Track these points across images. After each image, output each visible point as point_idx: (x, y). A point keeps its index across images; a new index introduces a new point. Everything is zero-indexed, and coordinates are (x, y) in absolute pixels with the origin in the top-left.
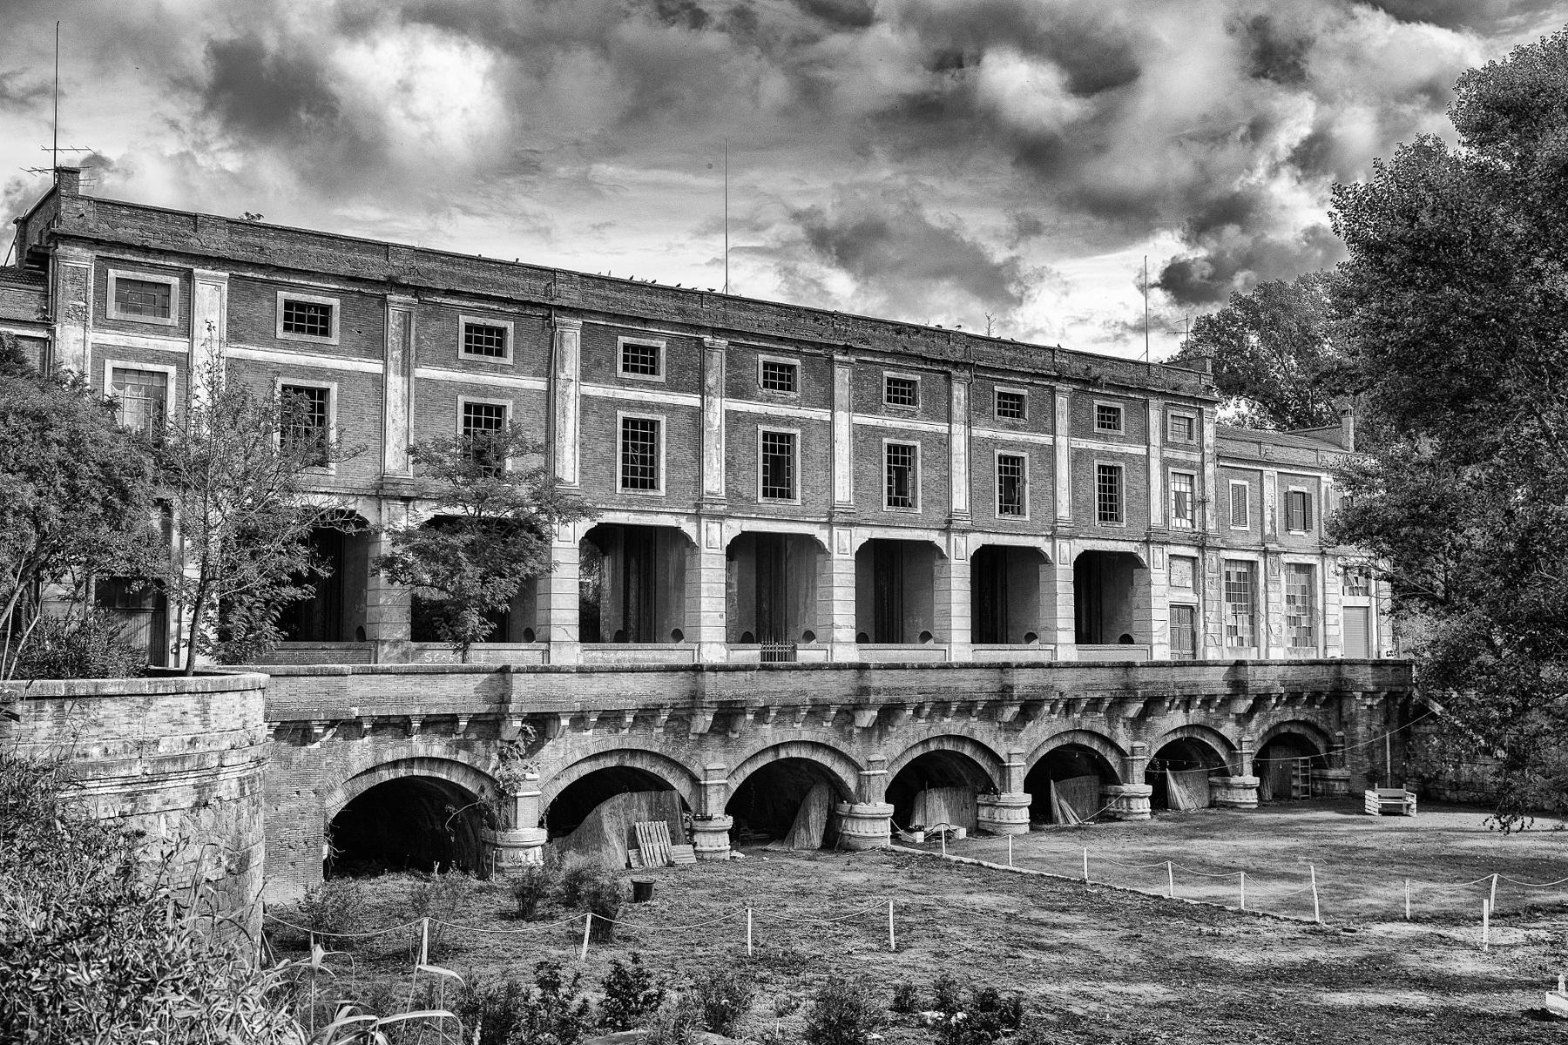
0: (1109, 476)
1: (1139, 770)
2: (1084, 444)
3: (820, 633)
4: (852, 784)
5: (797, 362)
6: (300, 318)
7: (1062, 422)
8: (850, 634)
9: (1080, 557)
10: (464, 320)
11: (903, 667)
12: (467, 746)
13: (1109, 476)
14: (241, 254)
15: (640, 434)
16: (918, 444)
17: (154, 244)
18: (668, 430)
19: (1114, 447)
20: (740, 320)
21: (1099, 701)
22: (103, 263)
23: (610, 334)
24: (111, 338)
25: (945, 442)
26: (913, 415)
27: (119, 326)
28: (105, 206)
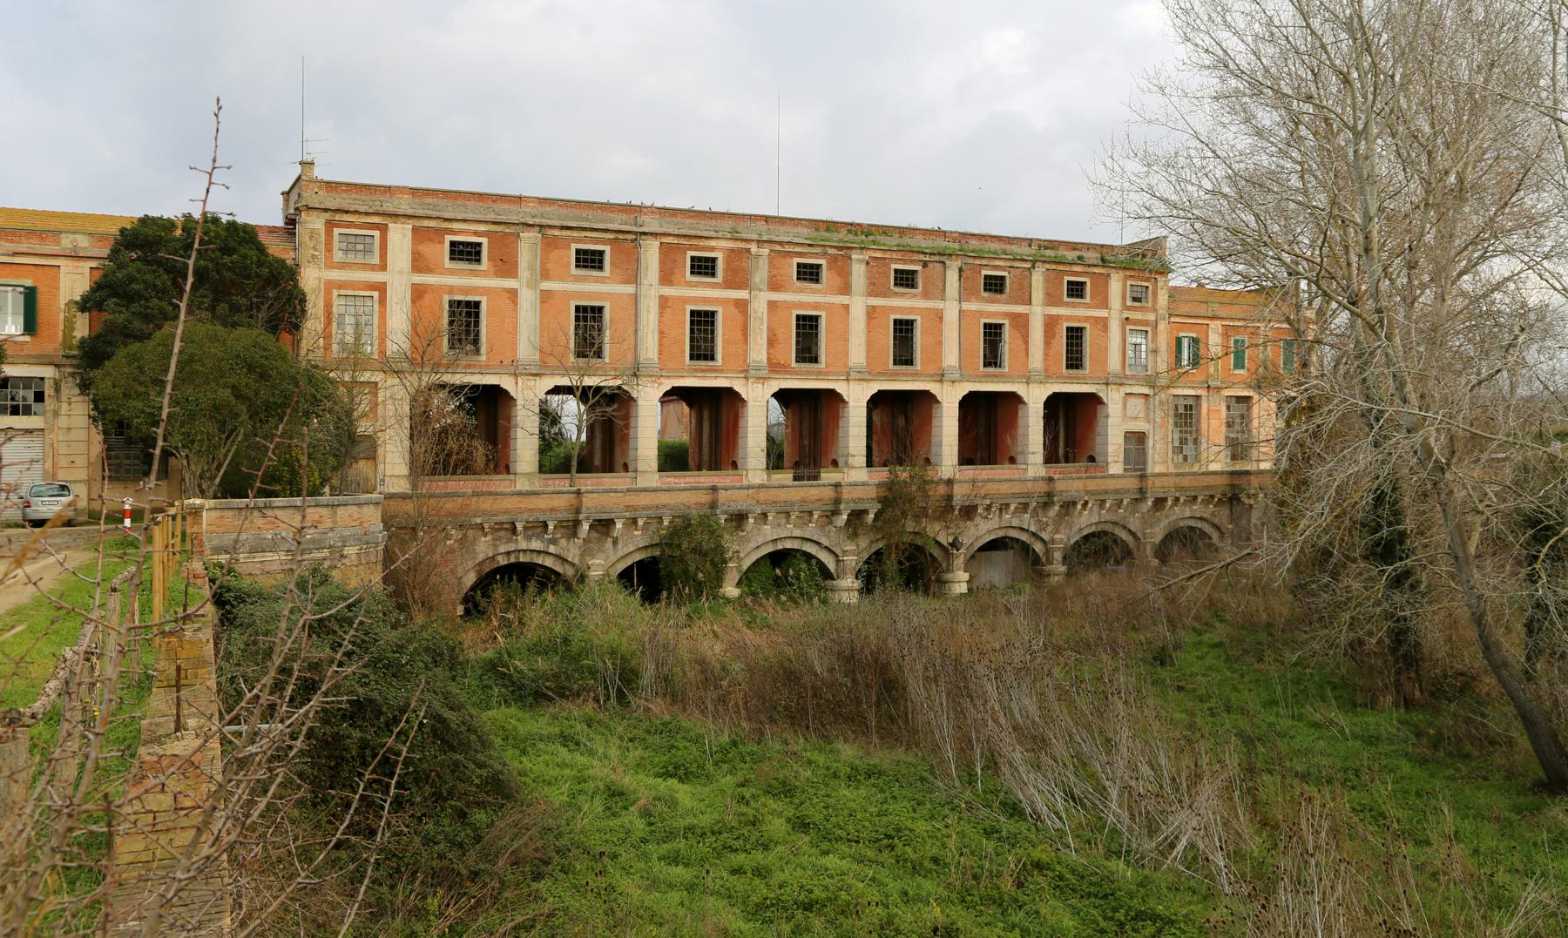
0: (1075, 335)
1: (1058, 556)
2: (1054, 311)
3: (841, 461)
4: (831, 566)
5: (822, 262)
6: (585, 260)
7: (1038, 293)
8: (1039, 458)
9: (1049, 398)
10: (574, 246)
11: (616, 491)
12: (554, 541)
13: (1075, 335)
14: (421, 212)
15: (703, 322)
16: (918, 318)
17: (362, 209)
18: (724, 318)
19: (1081, 312)
20: (783, 234)
21: (1212, 497)
22: (330, 225)
23: (681, 249)
24: (336, 275)
25: (939, 316)
26: (915, 296)
27: (343, 266)
28: (330, 186)
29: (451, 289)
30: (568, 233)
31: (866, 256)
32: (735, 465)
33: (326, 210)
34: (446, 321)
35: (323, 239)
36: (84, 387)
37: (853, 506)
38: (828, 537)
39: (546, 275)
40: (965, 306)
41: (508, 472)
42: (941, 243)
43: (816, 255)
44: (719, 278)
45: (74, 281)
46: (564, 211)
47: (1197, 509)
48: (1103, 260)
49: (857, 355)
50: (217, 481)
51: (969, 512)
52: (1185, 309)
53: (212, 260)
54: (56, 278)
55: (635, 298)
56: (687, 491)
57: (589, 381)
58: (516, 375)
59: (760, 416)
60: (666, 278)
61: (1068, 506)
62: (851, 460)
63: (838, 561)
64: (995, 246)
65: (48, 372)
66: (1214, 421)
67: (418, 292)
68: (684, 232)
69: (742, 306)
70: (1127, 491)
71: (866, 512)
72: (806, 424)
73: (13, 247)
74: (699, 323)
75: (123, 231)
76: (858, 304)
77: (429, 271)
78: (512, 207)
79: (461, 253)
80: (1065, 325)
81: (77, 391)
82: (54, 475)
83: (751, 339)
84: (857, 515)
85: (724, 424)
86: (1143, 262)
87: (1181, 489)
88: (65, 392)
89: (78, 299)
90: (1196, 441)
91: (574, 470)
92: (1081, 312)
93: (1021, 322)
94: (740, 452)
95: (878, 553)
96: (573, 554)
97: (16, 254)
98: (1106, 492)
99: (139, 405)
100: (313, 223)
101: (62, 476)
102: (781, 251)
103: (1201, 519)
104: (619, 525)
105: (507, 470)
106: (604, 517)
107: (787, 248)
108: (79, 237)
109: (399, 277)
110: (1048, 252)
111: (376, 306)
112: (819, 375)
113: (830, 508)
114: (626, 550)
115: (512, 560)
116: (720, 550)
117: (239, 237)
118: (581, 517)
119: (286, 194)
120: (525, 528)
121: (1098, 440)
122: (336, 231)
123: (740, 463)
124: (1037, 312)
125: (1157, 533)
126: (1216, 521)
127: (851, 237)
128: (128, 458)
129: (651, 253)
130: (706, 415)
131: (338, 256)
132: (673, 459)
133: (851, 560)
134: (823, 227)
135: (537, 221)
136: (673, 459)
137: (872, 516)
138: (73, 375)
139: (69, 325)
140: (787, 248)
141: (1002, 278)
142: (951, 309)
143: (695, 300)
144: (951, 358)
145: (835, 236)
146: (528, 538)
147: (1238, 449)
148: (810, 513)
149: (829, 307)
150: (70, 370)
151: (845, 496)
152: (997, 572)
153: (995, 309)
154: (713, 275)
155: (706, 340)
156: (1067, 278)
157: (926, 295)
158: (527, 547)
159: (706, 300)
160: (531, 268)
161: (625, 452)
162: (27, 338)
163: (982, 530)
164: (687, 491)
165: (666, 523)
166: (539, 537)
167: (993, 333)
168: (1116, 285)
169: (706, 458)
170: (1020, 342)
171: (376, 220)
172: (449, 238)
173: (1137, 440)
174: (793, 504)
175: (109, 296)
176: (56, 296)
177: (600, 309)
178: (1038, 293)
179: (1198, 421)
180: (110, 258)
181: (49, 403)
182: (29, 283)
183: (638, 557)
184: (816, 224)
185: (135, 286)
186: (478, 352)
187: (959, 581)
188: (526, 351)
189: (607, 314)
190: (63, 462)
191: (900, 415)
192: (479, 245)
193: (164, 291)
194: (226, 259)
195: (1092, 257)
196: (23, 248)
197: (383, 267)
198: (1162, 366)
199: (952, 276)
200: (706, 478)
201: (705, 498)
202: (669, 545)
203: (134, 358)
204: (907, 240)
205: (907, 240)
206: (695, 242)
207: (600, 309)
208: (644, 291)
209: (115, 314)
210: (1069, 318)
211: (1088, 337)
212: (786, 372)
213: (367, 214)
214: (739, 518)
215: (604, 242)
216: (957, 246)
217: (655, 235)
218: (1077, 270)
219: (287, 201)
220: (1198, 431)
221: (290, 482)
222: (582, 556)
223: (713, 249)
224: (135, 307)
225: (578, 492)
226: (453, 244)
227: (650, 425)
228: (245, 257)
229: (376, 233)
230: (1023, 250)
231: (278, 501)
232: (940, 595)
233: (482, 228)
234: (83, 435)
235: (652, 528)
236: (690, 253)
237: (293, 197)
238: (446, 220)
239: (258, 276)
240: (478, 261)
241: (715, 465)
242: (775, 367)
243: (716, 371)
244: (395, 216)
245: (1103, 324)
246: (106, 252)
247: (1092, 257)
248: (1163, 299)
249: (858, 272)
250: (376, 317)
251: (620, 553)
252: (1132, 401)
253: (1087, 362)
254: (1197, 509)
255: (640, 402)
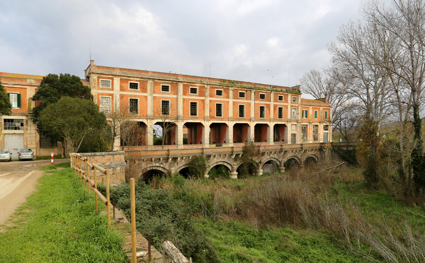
0: (280, 109)
1: (283, 165)
2: (276, 103)
3: (227, 142)
4: (230, 169)
7: (272, 99)
9: (255, 126)
10: (161, 85)
12: (162, 164)
13: (280, 109)
14: (122, 75)
17: (107, 73)
19: (282, 104)
20: (213, 82)
22: (99, 78)
23: (188, 86)
24: (100, 91)
25: (250, 104)
27: (102, 89)
28: (99, 67)
29: (131, 96)
30: (160, 81)
31: (233, 88)
32: (201, 143)
33: (97, 74)
34: (129, 104)
35: (97, 82)
36: (34, 121)
37: (237, 153)
38: (230, 161)
39: (154, 92)
40: (256, 102)
41: (145, 145)
42: (250, 86)
43: (221, 88)
44: (197, 94)
45: (31, 92)
46: (159, 75)
47: (313, 152)
48: (287, 91)
49: (231, 115)
50: (79, 147)
51: (263, 154)
52: (304, 103)
53: (69, 86)
54: (26, 92)
55: (177, 99)
56: (193, 150)
57: (167, 121)
58: (147, 119)
59: (181, 132)
60: (185, 93)
61: (286, 152)
62: (229, 141)
63: (232, 167)
64: (263, 87)
65: (24, 118)
66: (310, 131)
67: (122, 97)
68: (189, 81)
69: (203, 101)
70: (298, 148)
71: (239, 154)
72: (217, 132)
73: (14, 83)
74: (193, 105)
75: (44, 78)
76: (231, 101)
77: (124, 91)
78: (146, 74)
79: (133, 86)
80: (278, 107)
81: (32, 123)
82: (27, 146)
83: (205, 110)
84: (237, 155)
85: (198, 132)
86: (296, 91)
87: (310, 147)
88: (29, 123)
89: (32, 97)
90: (306, 136)
91: (163, 144)
92: (282, 104)
93: (268, 106)
94: (203, 140)
95: (242, 165)
96: (167, 167)
97: (15, 85)
98: (294, 148)
99: (55, 123)
100: (94, 77)
101: (29, 147)
102: (212, 87)
103: (314, 155)
104: (179, 159)
105: (145, 144)
106: (175, 157)
107: (214, 86)
108: (32, 80)
109: (117, 92)
110: (274, 88)
111: (111, 100)
112: (222, 119)
113: (231, 153)
114: (180, 166)
115: (151, 169)
116: (204, 165)
117: (76, 80)
118: (170, 157)
119: (86, 71)
120: (155, 160)
121: (285, 136)
122: (100, 79)
123: (202, 142)
124: (272, 104)
125: (304, 159)
126: (317, 155)
127: (229, 84)
128: (46, 141)
129: (181, 87)
130: (193, 130)
131: (101, 86)
132: (158, 142)
133: (236, 167)
134: (222, 81)
135: (152, 78)
136: (158, 142)
137: (241, 155)
138: (31, 118)
139: (30, 105)
140: (214, 86)
141: (264, 95)
142: (252, 102)
143: (192, 99)
144: (252, 115)
145: (225, 83)
146: (155, 163)
147: (315, 138)
148: (226, 155)
149: (224, 102)
150: (30, 117)
151: (234, 150)
152: (268, 170)
153: (262, 103)
154: (196, 93)
155: (194, 110)
156: (279, 95)
157: (247, 99)
158: (155, 165)
159: (194, 100)
160: (151, 90)
161: (174, 140)
162: (18, 108)
163: (265, 159)
164: (193, 150)
165: (190, 158)
166: (158, 162)
167: (262, 109)
168: (290, 97)
169: (193, 141)
170: (268, 111)
171: (111, 76)
172: (129, 82)
173: (294, 135)
174: (222, 152)
175: (41, 96)
176: (26, 97)
177: (168, 102)
178: (272, 99)
179: (307, 131)
180: (41, 86)
181: (25, 126)
182: (18, 93)
183: (183, 167)
184: (221, 80)
185: (48, 93)
186: (137, 113)
187: (261, 172)
188: (150, 112)
189: (170, 103)
190: (29, 143)
191: (240, 129)
192: (137, 84)
193: (56, 94)
194: (73, 85)
195: (284, 90)
196: (17, 83)
197: (113, 90)
198: (300, 118)
199: (253, 94)
200: (166, 147)
201: (200, 151)
202: (192, 164)
203: (52, 108)
204: (242, 85)
205: (242, 85)
206: (191, 84)
207: (168, 102)
208: (179, 97)
209: (43, 100)
210: (279, 105)
211: (283, 110)
212: (214, 119)
213: (108, 75)
214: (209, 156)
215: (169, 83)
216: (254, 86)
217: (182, 82)
218: (281, 93)
219: (86, 72)
220: (307, 134)
221: (100, 148)
222: (169, 167)
223: (196, 86)
224: (48, 98)
225: (168, 150)
226: (130, 83)
227: (181, 132)
228: (78, 85)
229: (111, 80)
230: (269, 88)
231: (98, 153)
232: (256, 176)
233: (138, 79)
234: (34, 135)
235: (187, 159)
236: (190, 87)
237: (88, 71)
238: (129, 77)
239: (81, 90)
240: (137, 88)
241: (169, 143)
242: (211, 117)
243: (197, 118)
244: (116, 76)
245: (287, 107)
246: (39, 84)
247: (284, 90)
248: (300, 101)
249: (231, 92)
250: (111, 103)
251: (179, 167)
252: (293, 126)
253: (283, 116)
254: (313, 152)
255: (178, 126)
